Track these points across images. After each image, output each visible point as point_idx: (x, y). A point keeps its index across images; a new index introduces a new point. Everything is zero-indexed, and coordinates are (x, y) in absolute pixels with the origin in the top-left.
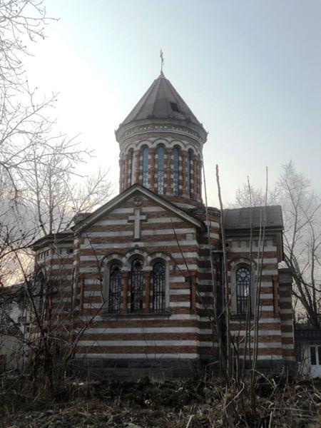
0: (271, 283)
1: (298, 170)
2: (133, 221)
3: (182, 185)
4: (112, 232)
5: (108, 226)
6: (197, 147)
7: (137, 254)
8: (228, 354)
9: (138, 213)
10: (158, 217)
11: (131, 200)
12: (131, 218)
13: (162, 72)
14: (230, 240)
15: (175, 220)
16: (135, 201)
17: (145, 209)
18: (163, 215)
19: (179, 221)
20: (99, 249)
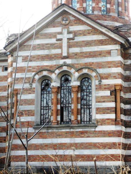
2: (61, 40)
5: (38, 45)
9: (65, 31)
11: (59, 19)
12: (59, 37)
15: (101, 37)
16: (63, 20)
18: (89, 33)
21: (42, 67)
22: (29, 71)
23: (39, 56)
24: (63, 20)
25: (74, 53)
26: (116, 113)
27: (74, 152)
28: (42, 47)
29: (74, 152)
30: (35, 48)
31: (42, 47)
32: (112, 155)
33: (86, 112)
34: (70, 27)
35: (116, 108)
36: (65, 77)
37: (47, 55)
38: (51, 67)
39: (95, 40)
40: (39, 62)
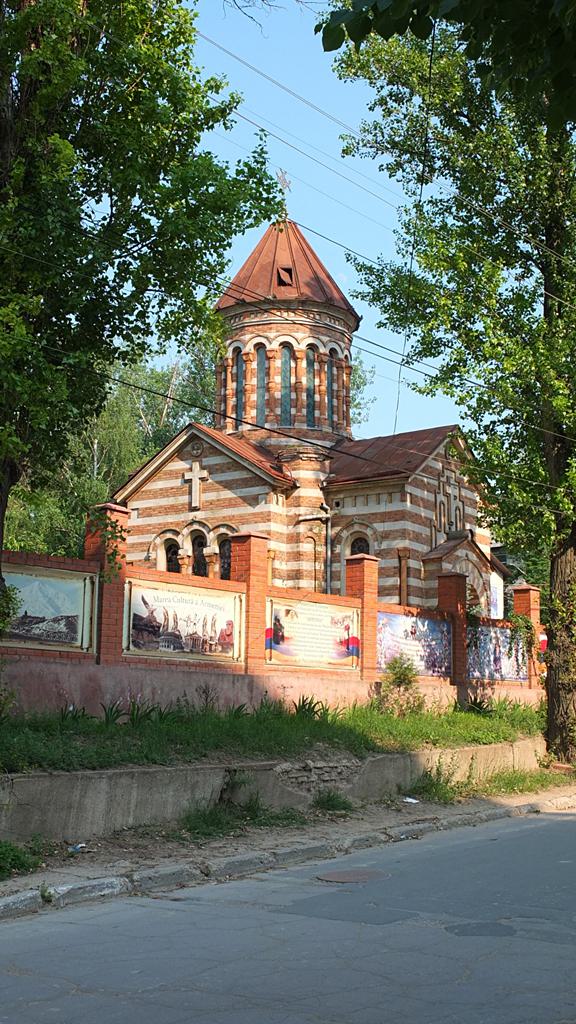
0: (397, 560)
1: (314, 32)
2: (190, 481)
3: (296, 407)
4: (166, 499)
5: (161, 489)
6: (343, 345)
7: (170, 539)
8: (58, 1010)
9: (196, 466)
10: (223, 472)
11: (189, 448)
12: (187, 476)
13: (361, 268)
14: (342, 496)
15: (244, 475)
16: (193, 449)
17: (206, 461)
18: (229, 469)
19: (250, 475)
20: (149, 525)
21: (165, 524)
22: (148, 532)
23: (161, 507)
24: (193, 449)
25: (207, 502)
26: (400, 595)
27: (261, 155)
28: (164, 493)
29: (261, 155)
30: (156, 494)
31: (164, 493)
32: (150, 515)
33: (383, 508)
34: (204, 460)
35: (400, 568)
36: (199, 541)
37: (172, 506)
38: (178, 524)
39: (237, 480)
40: (160, 518)
